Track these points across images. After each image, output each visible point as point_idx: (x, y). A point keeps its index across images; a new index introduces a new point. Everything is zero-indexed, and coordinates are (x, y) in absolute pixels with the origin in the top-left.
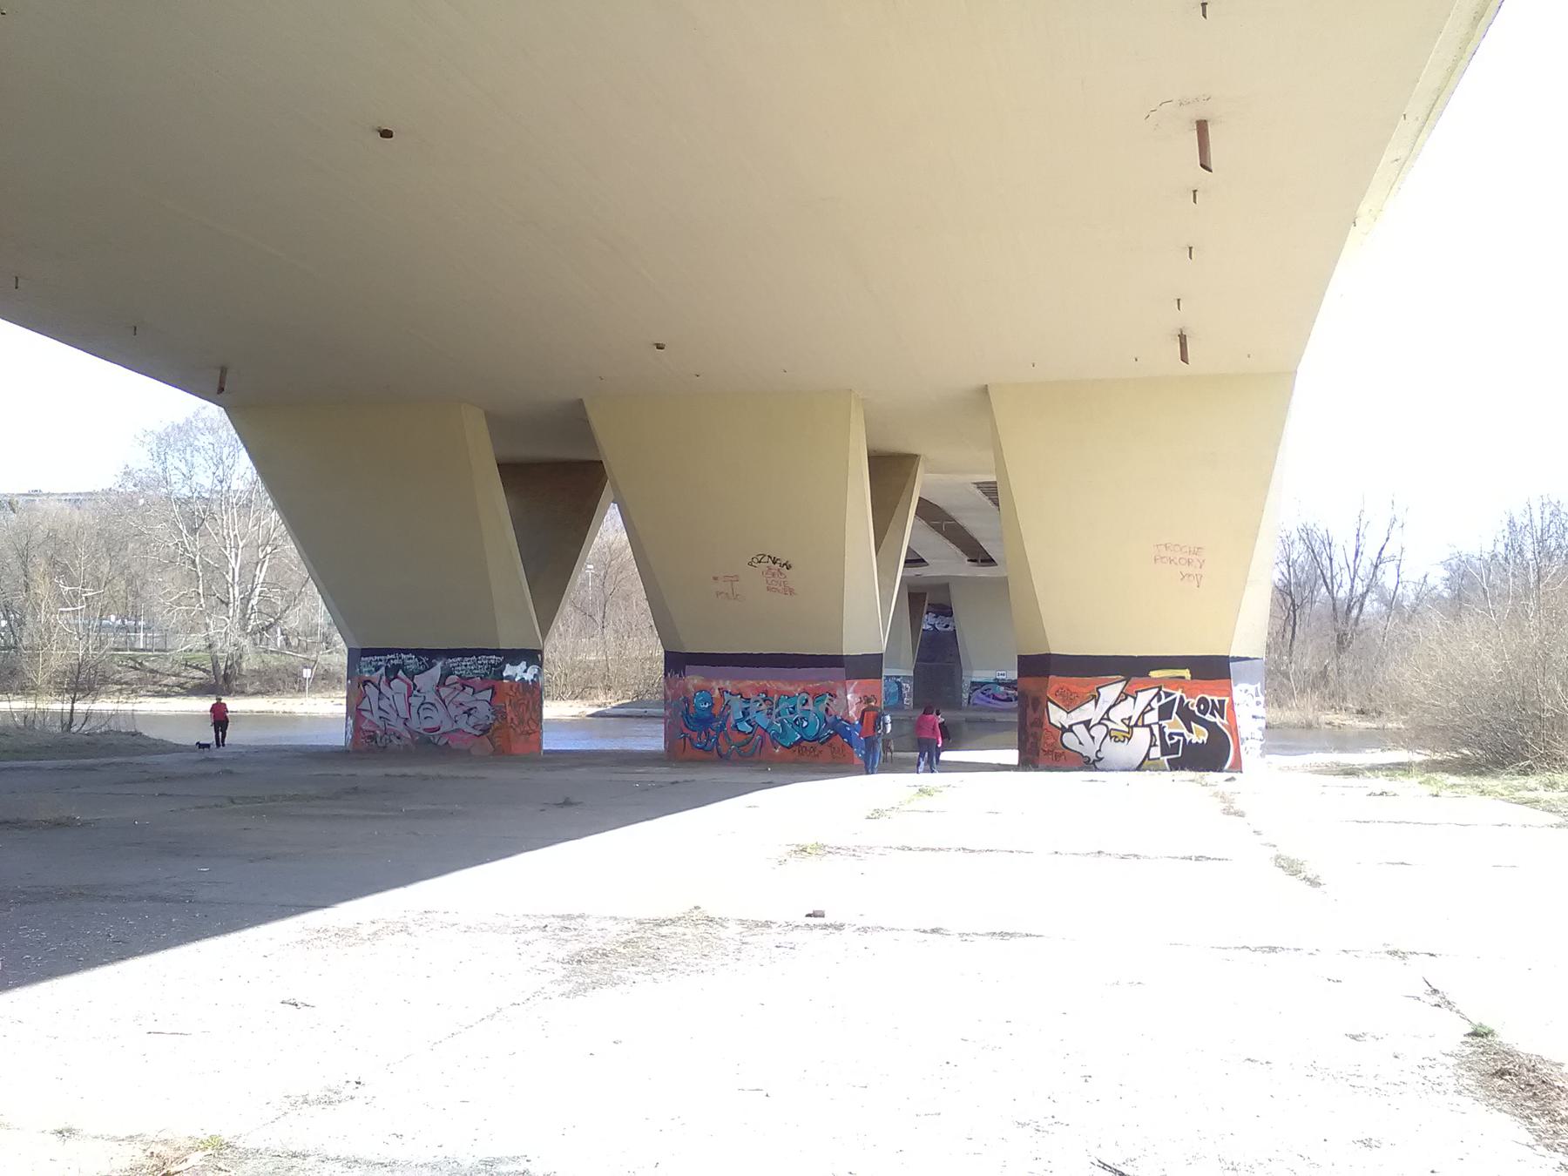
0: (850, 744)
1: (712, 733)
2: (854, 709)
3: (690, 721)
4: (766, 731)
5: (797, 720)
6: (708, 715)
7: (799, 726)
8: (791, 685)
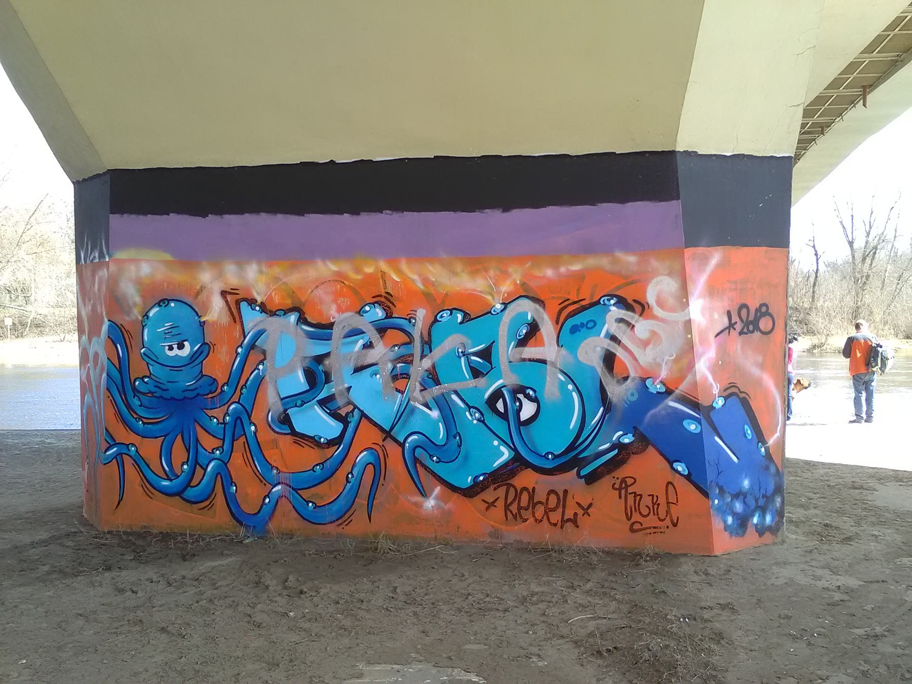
0: (696, 480)
1: (208, 442)
2: (711, 353)
3: (135, 402)
4: (388, 434)
5: (498, 394)
6: (186, 381)
7: (504, 416)
8: (474, 273)
